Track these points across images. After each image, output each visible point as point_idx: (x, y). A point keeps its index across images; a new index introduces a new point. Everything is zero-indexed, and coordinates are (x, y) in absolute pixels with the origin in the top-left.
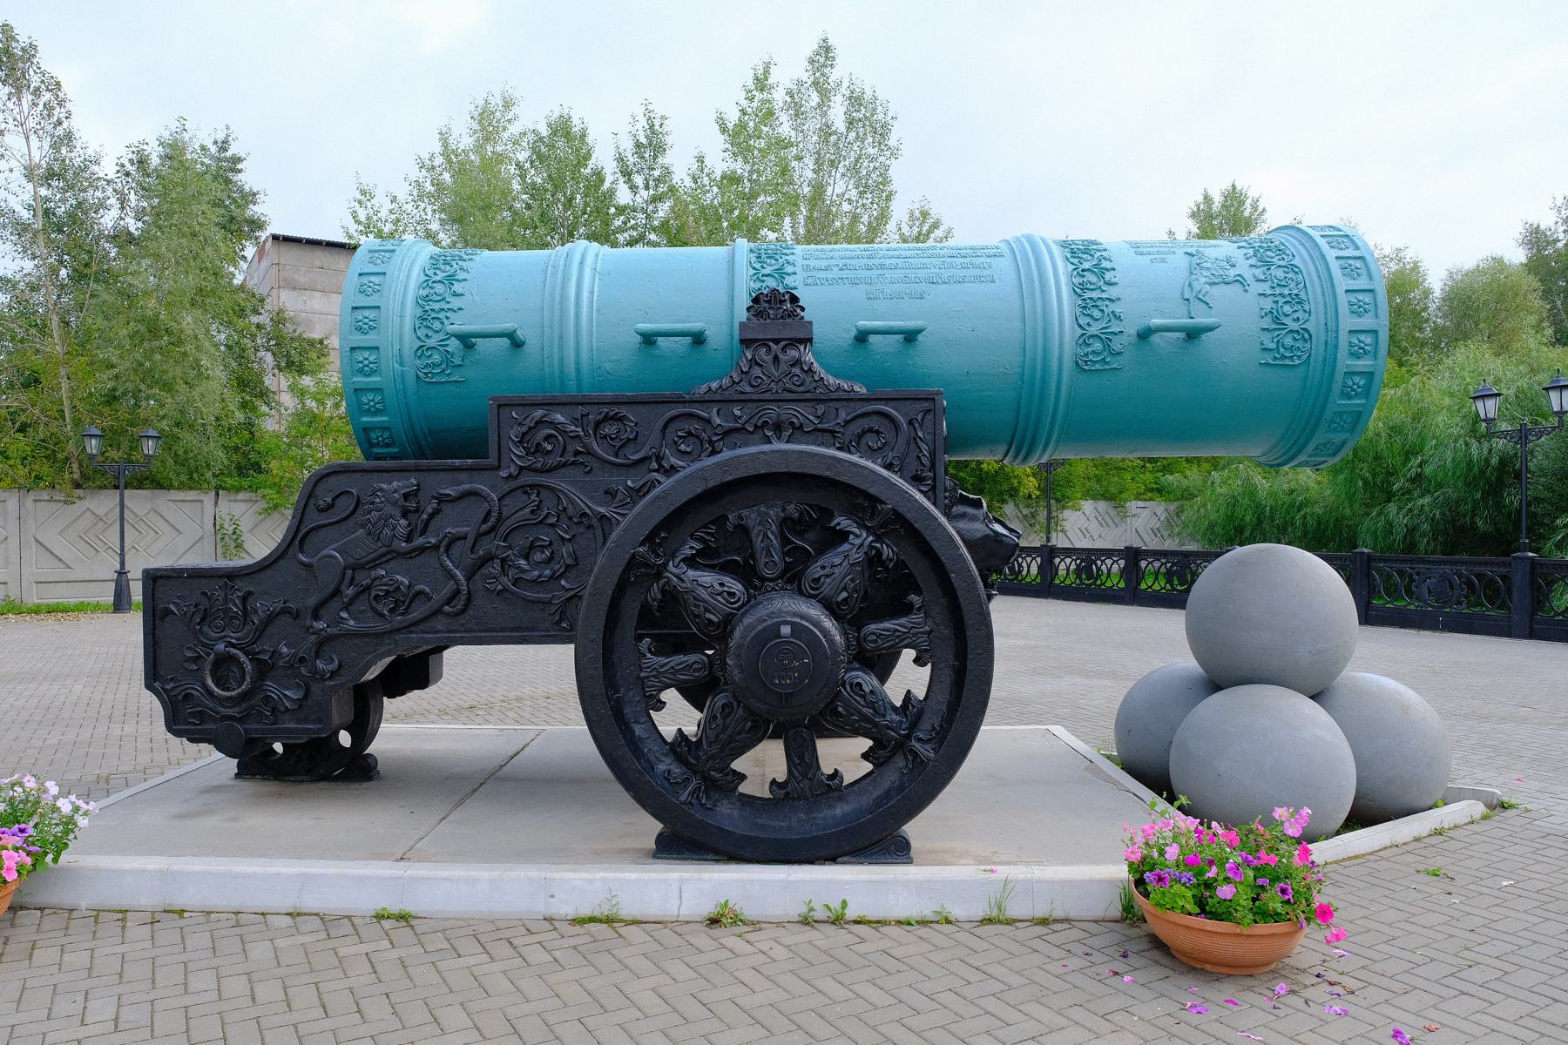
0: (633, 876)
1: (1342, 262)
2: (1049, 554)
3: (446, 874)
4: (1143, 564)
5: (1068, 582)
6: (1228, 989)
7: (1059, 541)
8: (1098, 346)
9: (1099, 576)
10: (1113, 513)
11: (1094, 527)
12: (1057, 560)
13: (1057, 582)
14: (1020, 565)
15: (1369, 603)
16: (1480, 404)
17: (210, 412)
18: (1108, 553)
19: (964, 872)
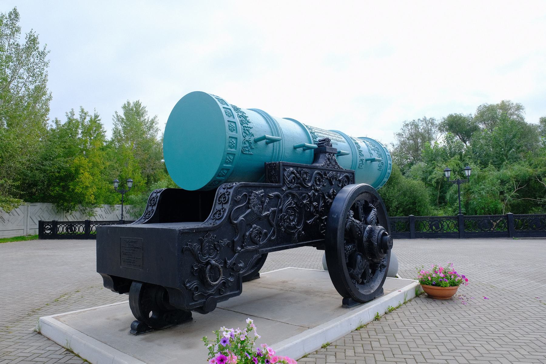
0: (361, 312)
1: (229, 123)
2: (88, 224)
3: (331, 326)
4: (91, 226)
5: (63, 233)
6: (439, 302)
7: (93, 219)
8: (247, 144)
9: (75, 230)
10: (110, 209)
11: (103, 214)
12: (58, 226)
13: (91, 233)
14: (75, 228)
15: (458, 221)
16: (446, 173)
17: (145, 118)
18: (79, 223)
19: (396, 293)
